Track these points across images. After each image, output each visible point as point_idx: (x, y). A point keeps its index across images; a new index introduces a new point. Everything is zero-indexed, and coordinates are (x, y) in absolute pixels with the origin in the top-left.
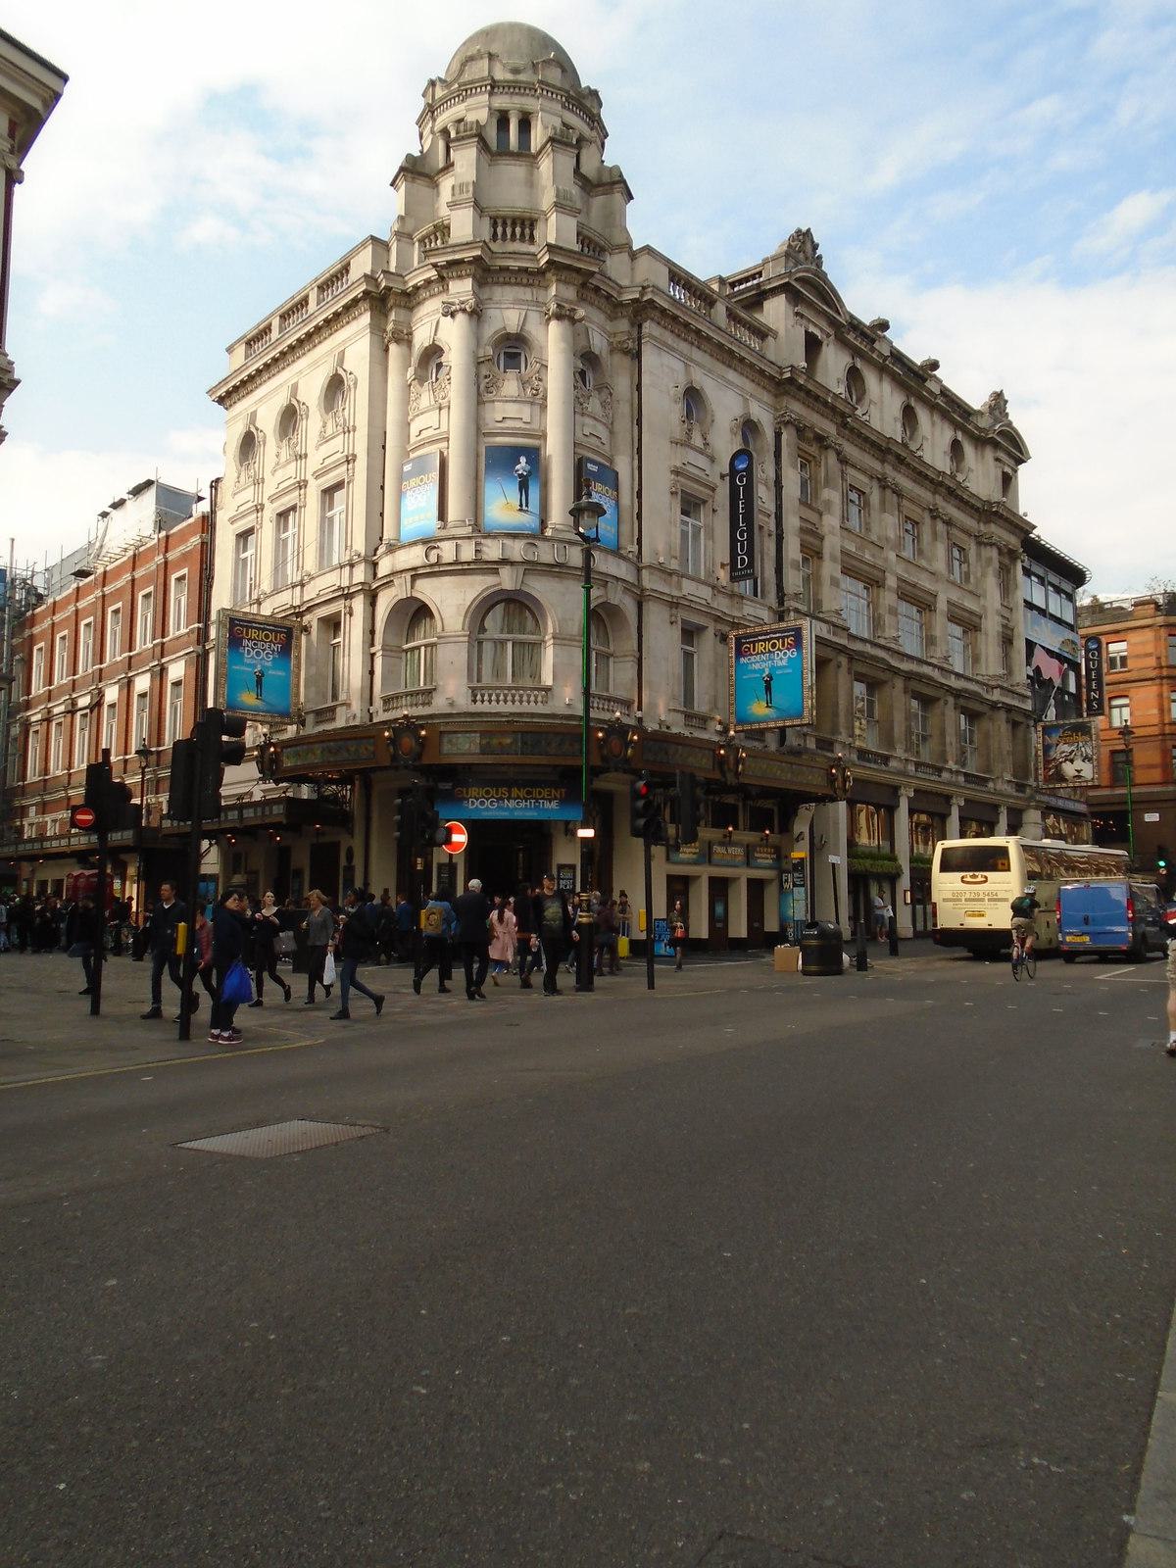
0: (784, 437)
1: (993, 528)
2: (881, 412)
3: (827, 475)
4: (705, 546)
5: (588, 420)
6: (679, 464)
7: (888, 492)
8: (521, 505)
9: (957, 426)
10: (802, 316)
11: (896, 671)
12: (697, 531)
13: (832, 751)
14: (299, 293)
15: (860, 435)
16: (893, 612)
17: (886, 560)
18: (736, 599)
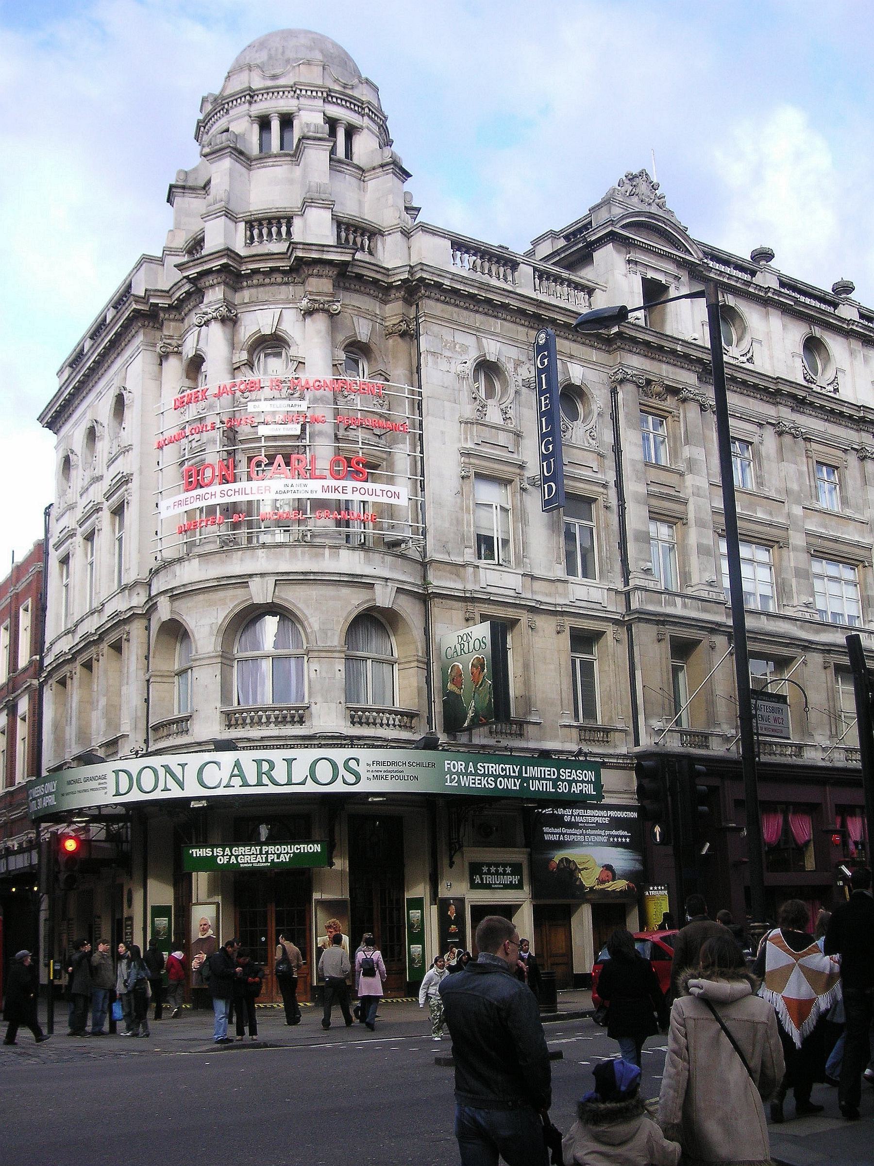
0: (620, 396)
6: (470, 445)
7: (787, 439)
11: (808, 646)
13: (707, 747)
16: (804, 574)
17: (789, 515)
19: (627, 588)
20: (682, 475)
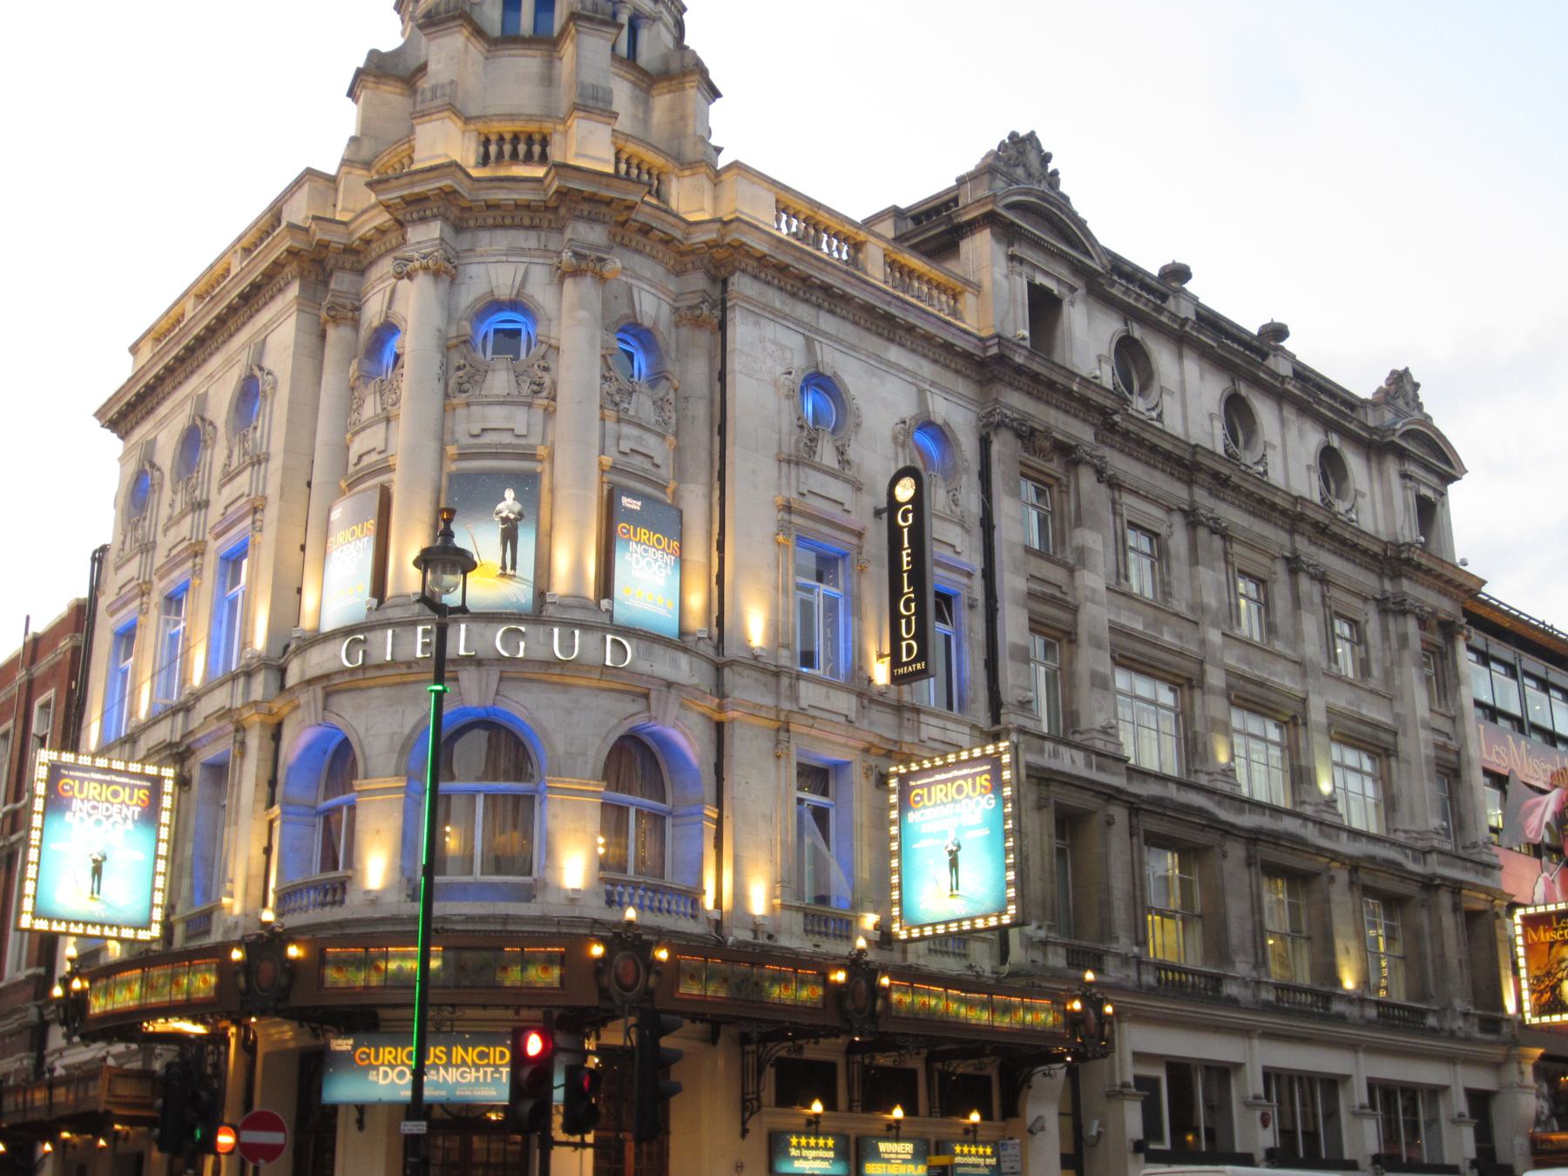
0: (995, 448)
1: (1406, 586)
2: (1184, 405)
3: (1078, 507)
4: (846, 626)
5: (627, 430)
7: (1202, 533)
8: (504, 567)
9: (1328, 426)
10: (1021, 261)
11: (1228, 831)
12: (831, 605)
14: (218, 260)
15: (1140, 442)
17: (1203, 642)
18: (907, 715)
19: (997, 728)
20: (1071, 571)
